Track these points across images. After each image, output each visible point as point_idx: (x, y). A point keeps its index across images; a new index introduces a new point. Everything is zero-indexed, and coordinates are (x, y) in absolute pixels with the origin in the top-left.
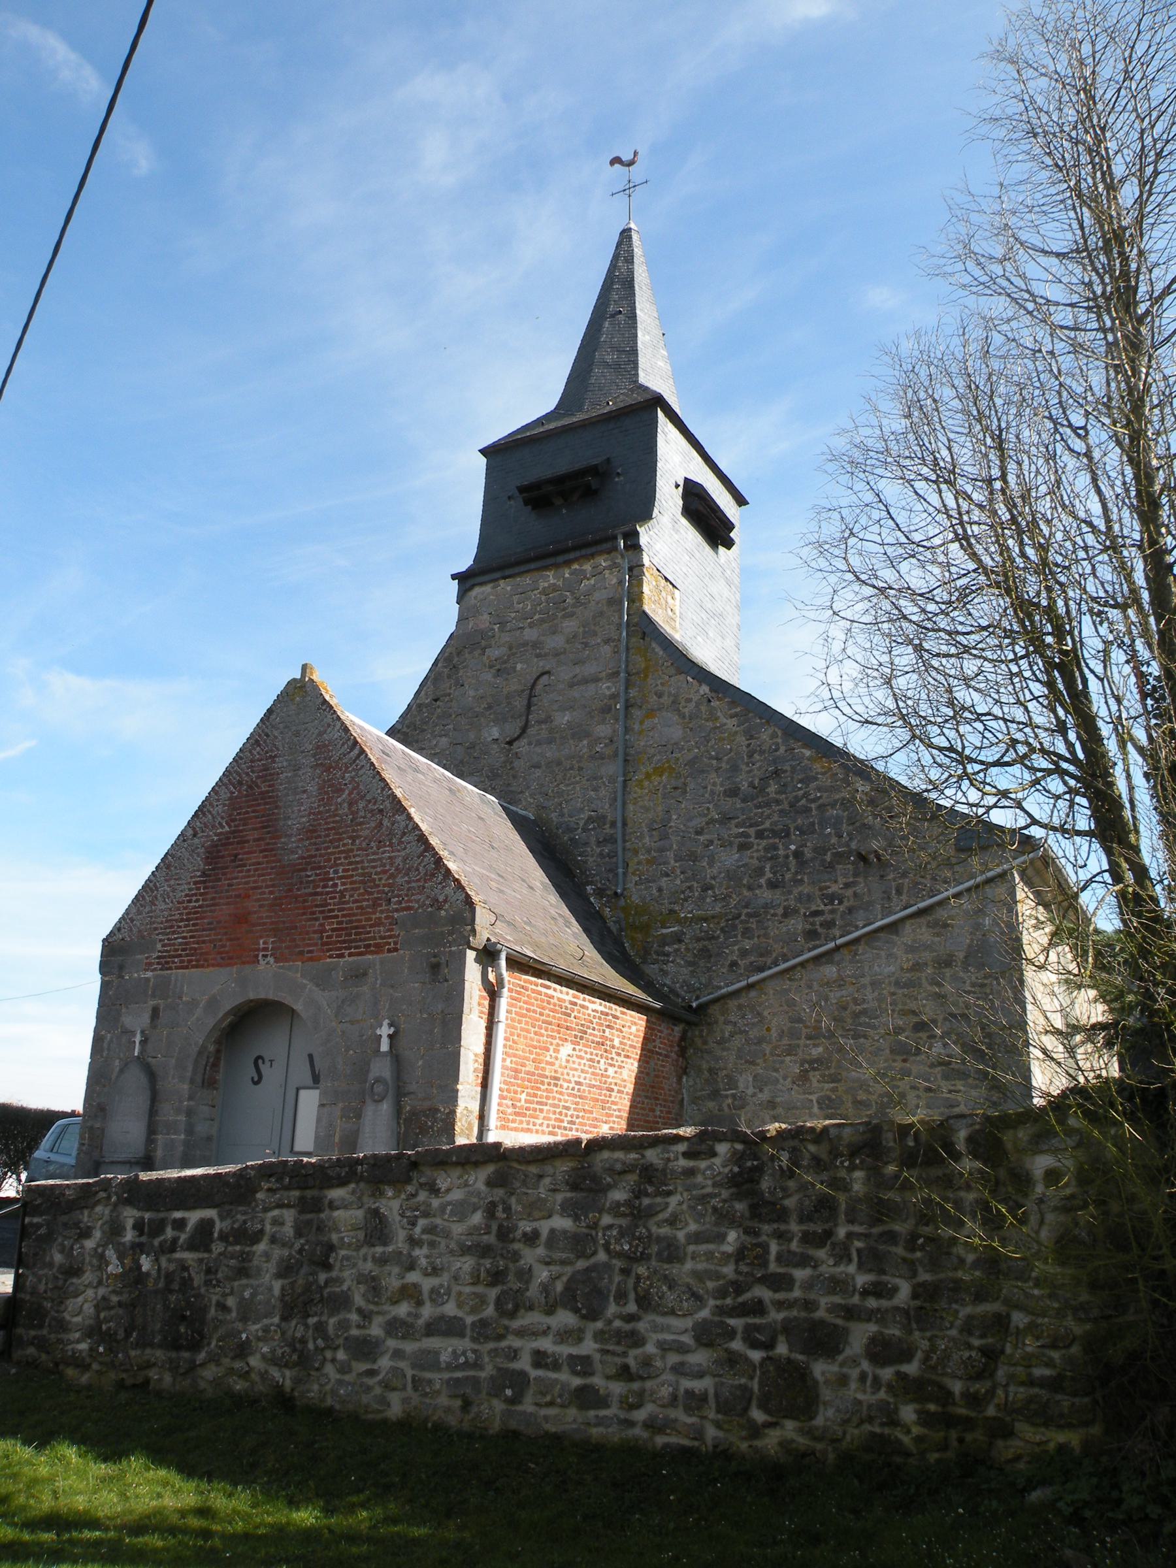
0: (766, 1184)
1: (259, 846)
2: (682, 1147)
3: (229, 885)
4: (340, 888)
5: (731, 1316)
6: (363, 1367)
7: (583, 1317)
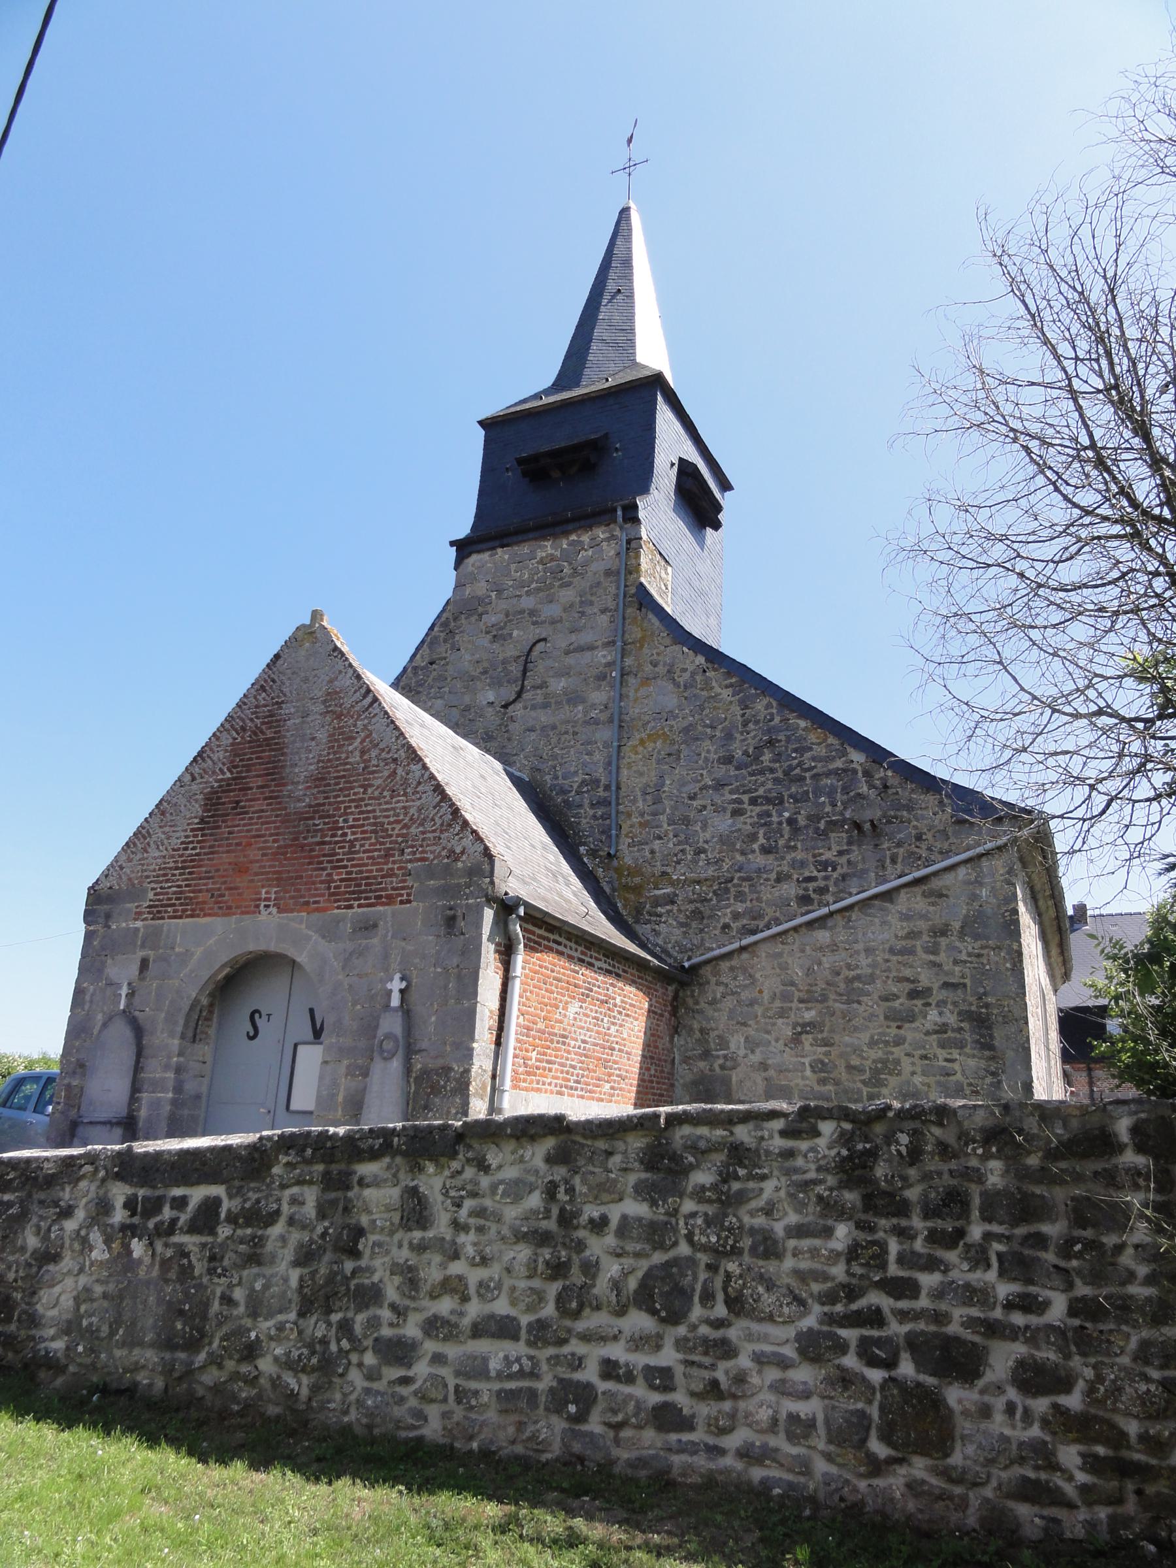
0: (881, 1171)
1: (262, 793)
2: (778, 1124)
3: (230, 833)
4: (349, 837)
5: (842, 1326)
6: (395, 1373)
7: (663, 1320)
